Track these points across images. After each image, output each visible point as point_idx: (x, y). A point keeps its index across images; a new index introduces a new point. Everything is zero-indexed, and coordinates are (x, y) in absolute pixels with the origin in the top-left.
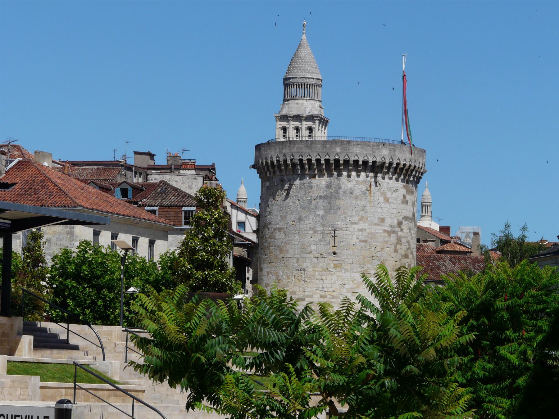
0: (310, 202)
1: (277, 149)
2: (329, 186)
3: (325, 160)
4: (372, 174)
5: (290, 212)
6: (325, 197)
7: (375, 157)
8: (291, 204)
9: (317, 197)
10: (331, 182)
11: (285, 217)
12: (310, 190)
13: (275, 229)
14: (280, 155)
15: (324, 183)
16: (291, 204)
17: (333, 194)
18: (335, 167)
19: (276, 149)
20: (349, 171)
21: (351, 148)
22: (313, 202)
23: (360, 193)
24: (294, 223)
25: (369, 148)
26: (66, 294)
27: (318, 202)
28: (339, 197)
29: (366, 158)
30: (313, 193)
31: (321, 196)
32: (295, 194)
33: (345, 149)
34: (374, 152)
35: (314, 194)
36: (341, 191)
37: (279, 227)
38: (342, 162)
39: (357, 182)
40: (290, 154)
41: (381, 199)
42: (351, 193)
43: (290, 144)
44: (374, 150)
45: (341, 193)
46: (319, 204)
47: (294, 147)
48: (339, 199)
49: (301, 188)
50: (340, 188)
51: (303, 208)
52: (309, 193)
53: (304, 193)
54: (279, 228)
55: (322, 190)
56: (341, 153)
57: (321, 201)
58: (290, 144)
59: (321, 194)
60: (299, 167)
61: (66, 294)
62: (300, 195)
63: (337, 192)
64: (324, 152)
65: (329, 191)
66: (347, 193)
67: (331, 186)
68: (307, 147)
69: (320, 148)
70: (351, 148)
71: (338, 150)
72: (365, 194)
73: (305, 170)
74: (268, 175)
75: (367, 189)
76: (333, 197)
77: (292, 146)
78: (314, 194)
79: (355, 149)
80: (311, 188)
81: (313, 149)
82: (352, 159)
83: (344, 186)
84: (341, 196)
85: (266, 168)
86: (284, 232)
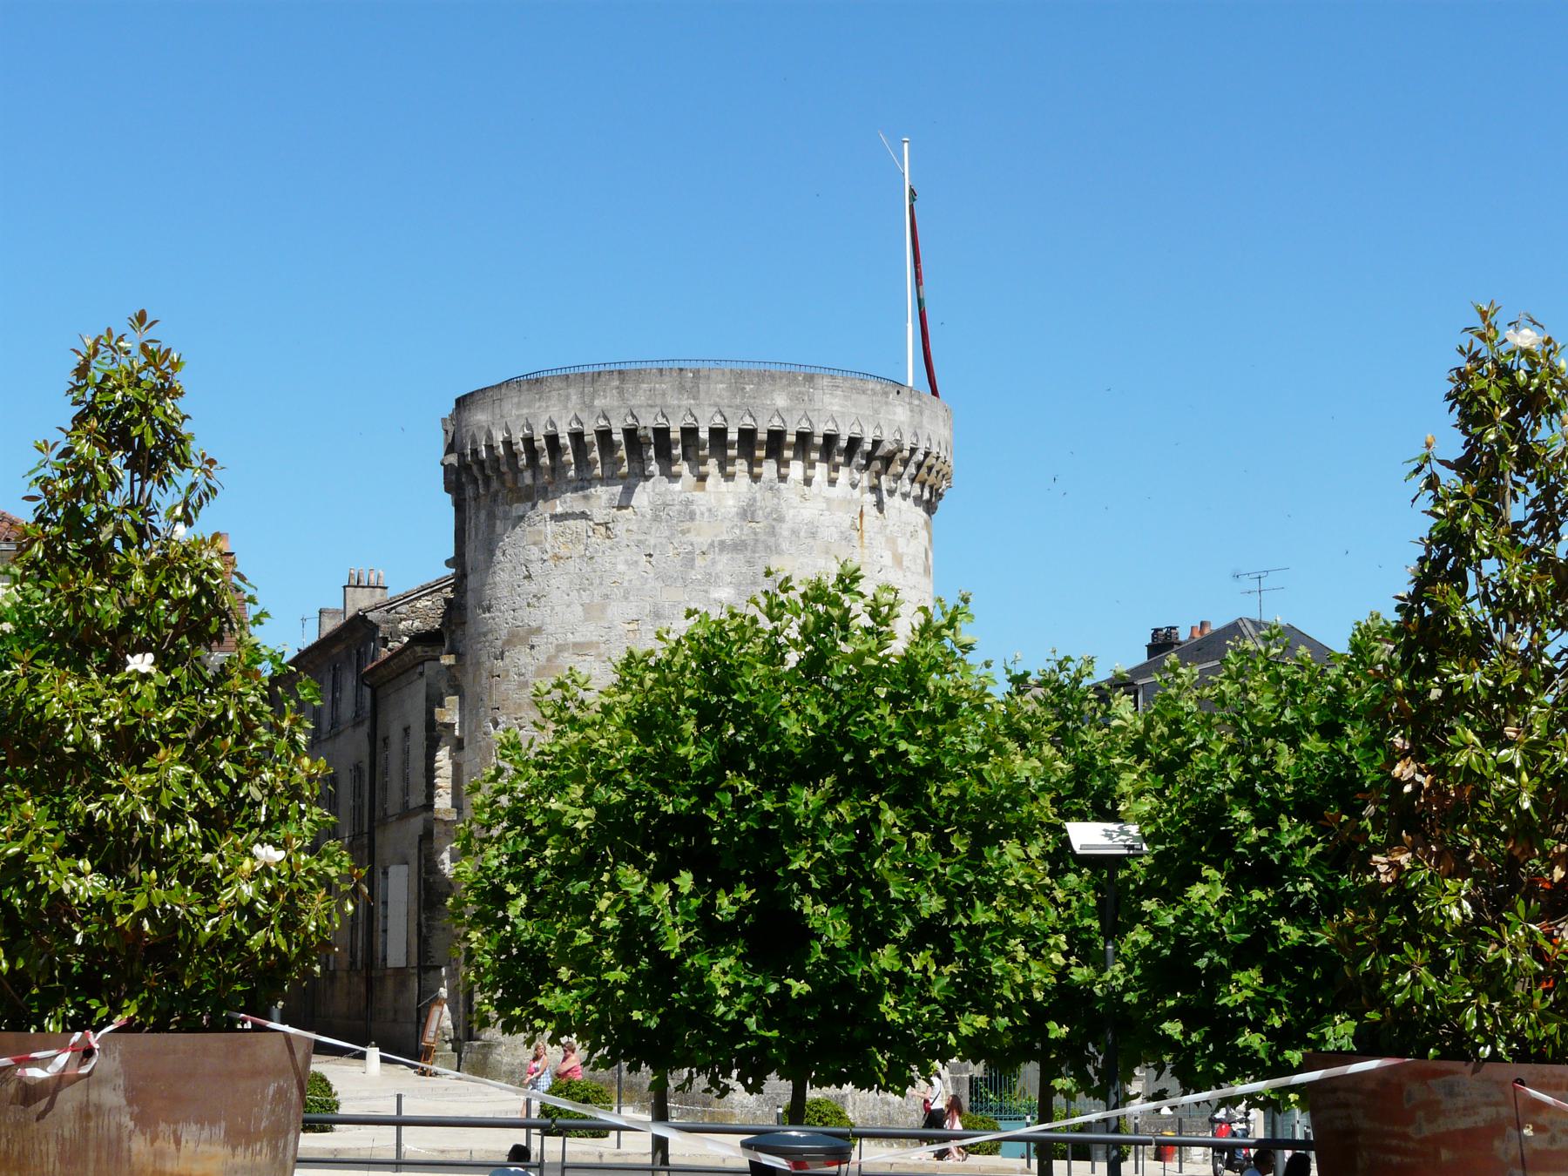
0: (689, 561)
1: (574, 398)
2: (747, 513)
3: (741, 431)
4: (865, 479)
5: (619, 593)
6: (738, 547)
7: (878, 426)
8: (621, 567)
9: (712, 545)
10: (755, 499)
11: (603, 609)
12: (686, 525)
13: (560, 648)
14: (583, 416)
15: (731, 502)
16: (621, 567)
17: (762, 537)
18: (650, 449)
19: (568, 397)
20: (753, 462)
21: (818, 395)
22: (699, 562)
23: (836, 536)
24: (631, 627)
25: (863, 398)
26: (1199, 1069)
27: (714, 562)
28: (777, 546)
29: (857, 430)
30: (698, 534)
31: (722, 543)
32: (635, 537)
33: (798, 398)
34: (876, 412)
35: (702, 536)
36: (784, 530)
37: (578, 638)
38: (791, 438)
39: (828, 500)
40: (624, 411)
41: (888, 559)
42: (813, 535)
43: (623, 381)
44: (876, 406)
45: (786, 533)
46: (719, 567)
47: (636, 389)
48: (779, 552)
49: (656, 518)
50: (780, 519)
51: (663, 578)
52: (683, 532)
53: (667, 533)
54: (575, 645)
55: (728, 524)
56: (788, 410)
57: (725, 558)
58: (623, 381)
59: (724, 537)
60: (652, 452)
61: (1199, 1069)
62: (652, 541)
63: (772, 532)
64: (738, 407)
65: (747, 526)
66: (802, 534)
67: (753, 513)
68: (682, 388)
69: (725, 394)
70: (818, 395)
71: (781, 401)
72: (848, 539)
73: (591, 465)
74: (527, 478)
75: (853, 524)
76: (761, 547)
77: (629, 386)
78: (702, 536)
79: (827, 399)
80: (692, 519)
81: (702, 395)
82: (821, 429)
83: (792, 512)
84: (785, 545)
85: (523, 460)
86: (599, 655)
